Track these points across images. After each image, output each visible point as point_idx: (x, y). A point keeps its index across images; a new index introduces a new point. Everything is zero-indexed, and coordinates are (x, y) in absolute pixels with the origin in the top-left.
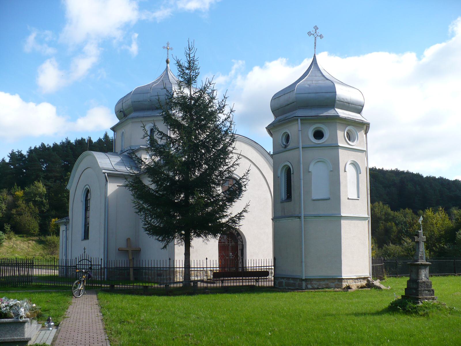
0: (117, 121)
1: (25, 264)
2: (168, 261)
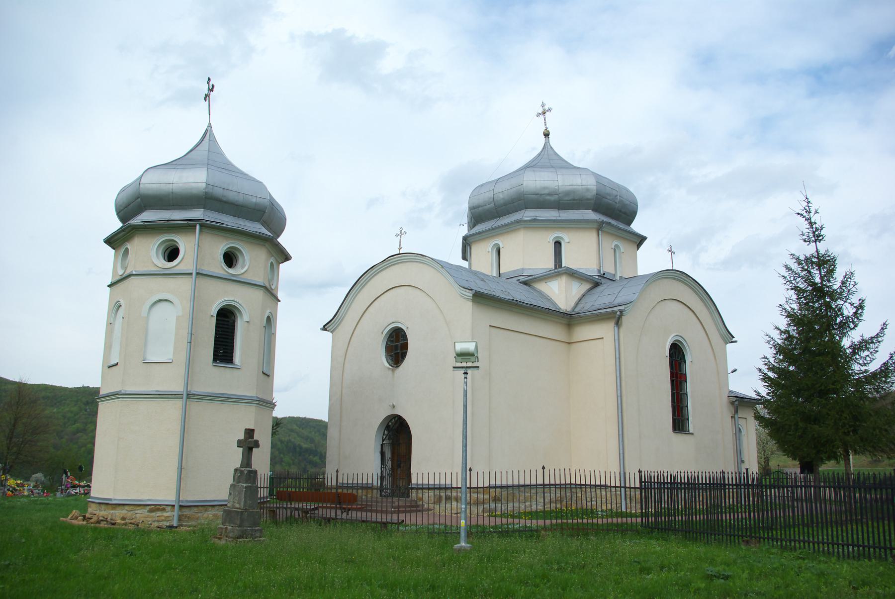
0: (117, 225)
1: (714, 489)
2: (540, 471)
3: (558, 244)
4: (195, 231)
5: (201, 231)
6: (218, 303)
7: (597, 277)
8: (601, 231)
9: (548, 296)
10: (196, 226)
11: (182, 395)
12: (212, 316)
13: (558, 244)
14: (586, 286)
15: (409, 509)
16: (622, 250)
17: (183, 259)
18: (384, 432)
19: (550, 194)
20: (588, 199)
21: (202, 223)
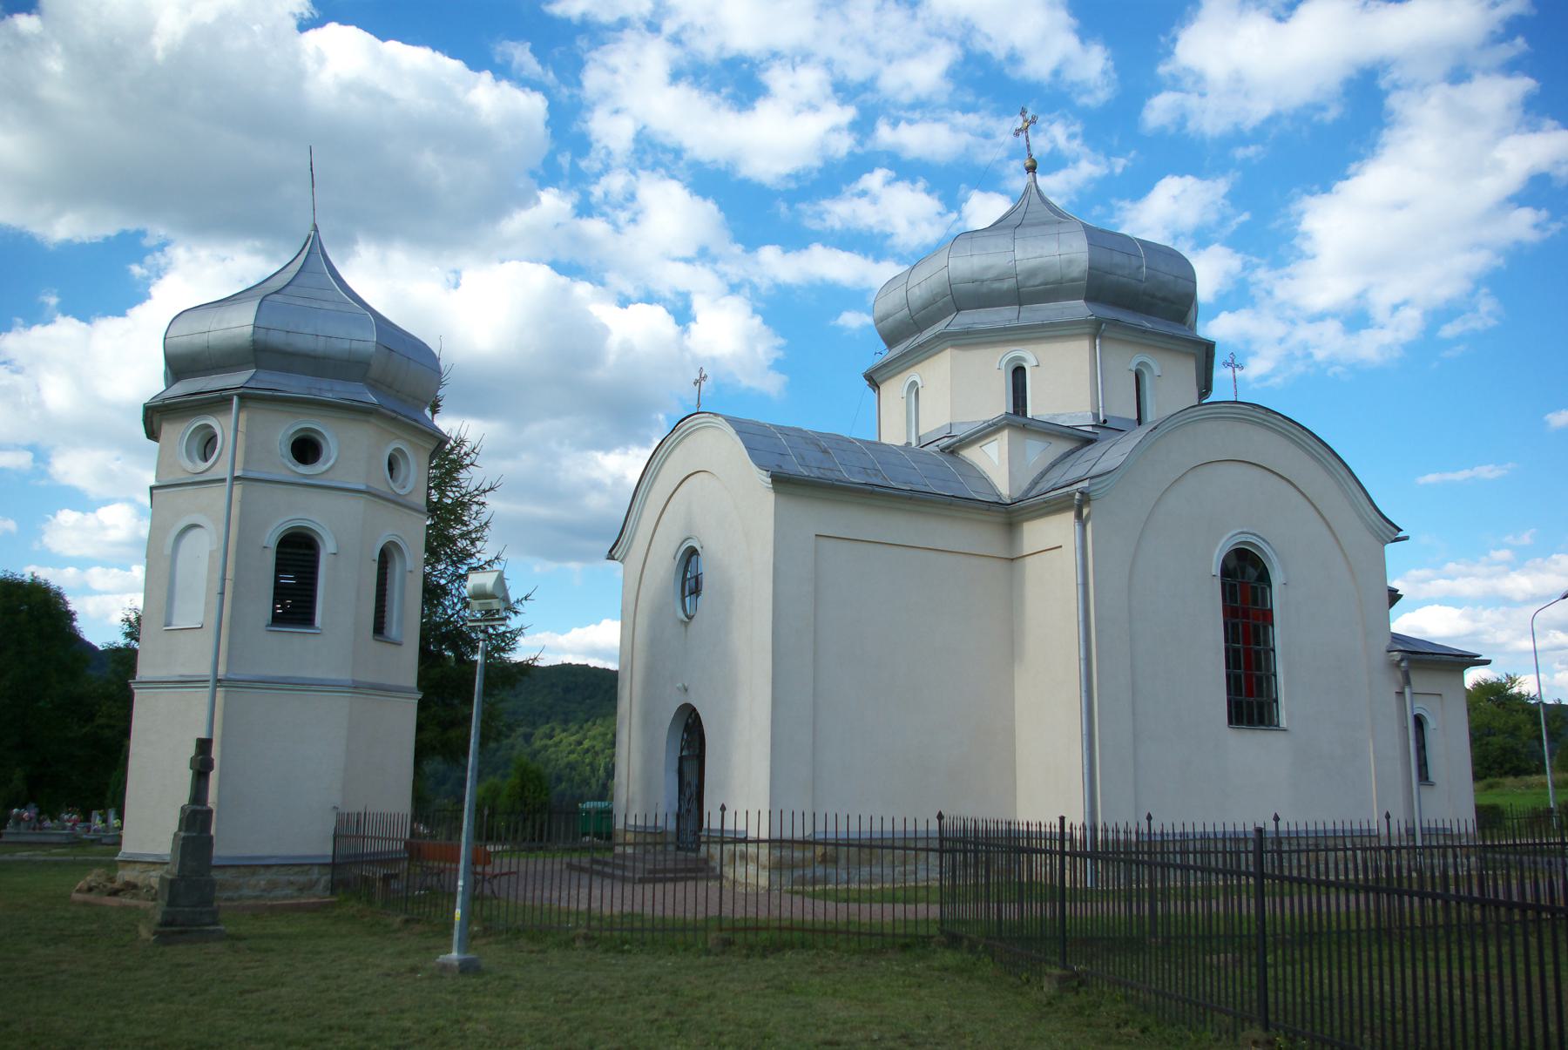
3: (1018, 374)
4: (231, 409)
5: (240, 408)
6: (276, 525)
7: (1090, 429)
8: (1101, 338)
9: (984, 472)
10: (232, 400)
11: (208, 681)
12: (265, 547)
13: (1018, 374)
14: (1062, 447)
15: (672, 875)
16: (1157, 371)
17: (222, 449)
18: (683, 735)
19: (999, 279)
20: (1073, 280)
21: (242, 393)
